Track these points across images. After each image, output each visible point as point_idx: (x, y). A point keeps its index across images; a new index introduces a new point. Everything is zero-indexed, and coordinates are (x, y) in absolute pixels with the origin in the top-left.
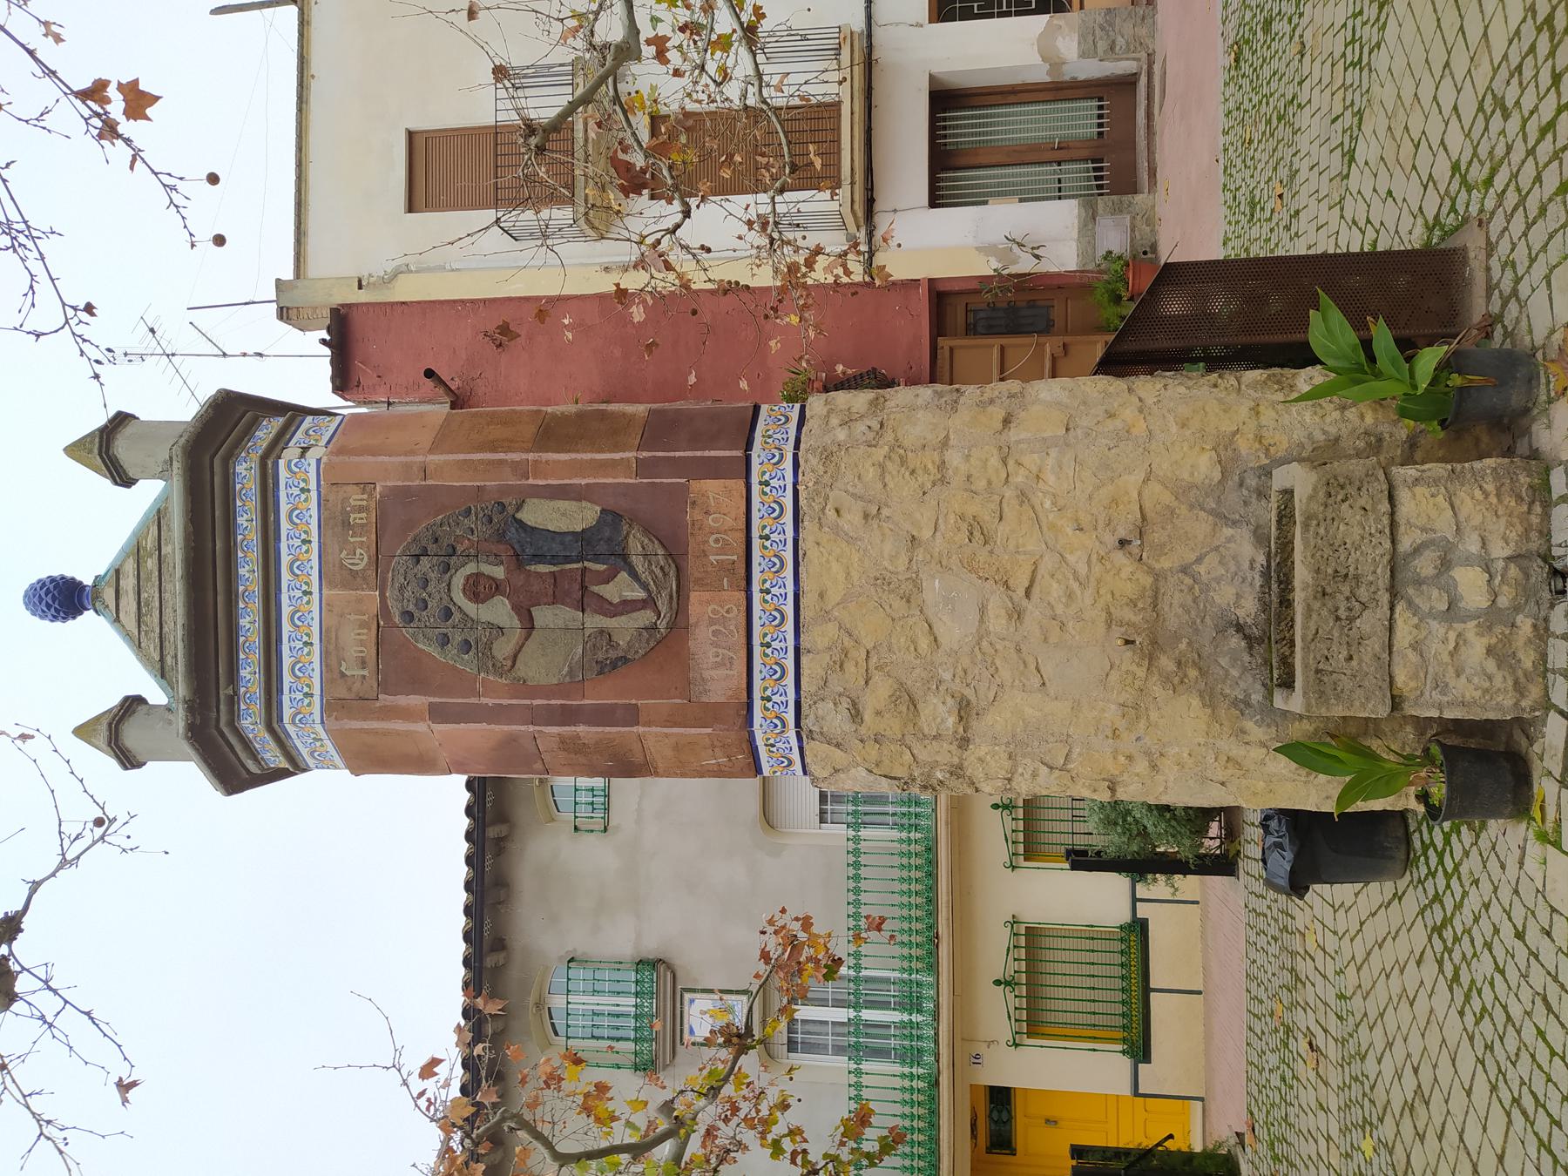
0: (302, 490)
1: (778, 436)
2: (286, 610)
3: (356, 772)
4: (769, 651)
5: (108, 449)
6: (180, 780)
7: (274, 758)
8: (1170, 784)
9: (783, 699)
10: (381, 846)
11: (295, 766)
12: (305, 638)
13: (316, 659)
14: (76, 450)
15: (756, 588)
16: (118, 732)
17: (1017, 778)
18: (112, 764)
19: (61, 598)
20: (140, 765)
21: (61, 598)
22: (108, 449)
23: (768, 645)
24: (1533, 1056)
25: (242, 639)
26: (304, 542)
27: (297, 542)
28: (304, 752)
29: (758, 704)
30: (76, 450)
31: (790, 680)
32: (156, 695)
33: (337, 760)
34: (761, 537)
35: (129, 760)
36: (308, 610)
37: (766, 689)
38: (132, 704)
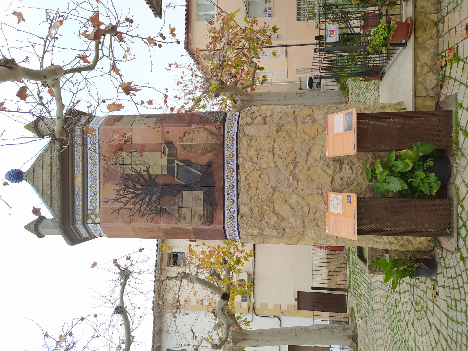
1: (233, 119)
2: (89, 170)
3: (111, 236)
4: (229, 196)
6: (58, 240)
11: (92, 237)
12: (94, 178)
14: (27, 227)
15: (226, 209)
18: (35, 237)
19: (16, 176)
20: (43, 236)
21: (16, 176)
25: (76, 193)
26: (95, 179)
27: (93, 180)
29: (226, 165)
31: (235, 189)
34: (227, 147)
35: (40, 235)
36: (95, 190)
37: (228, 191)
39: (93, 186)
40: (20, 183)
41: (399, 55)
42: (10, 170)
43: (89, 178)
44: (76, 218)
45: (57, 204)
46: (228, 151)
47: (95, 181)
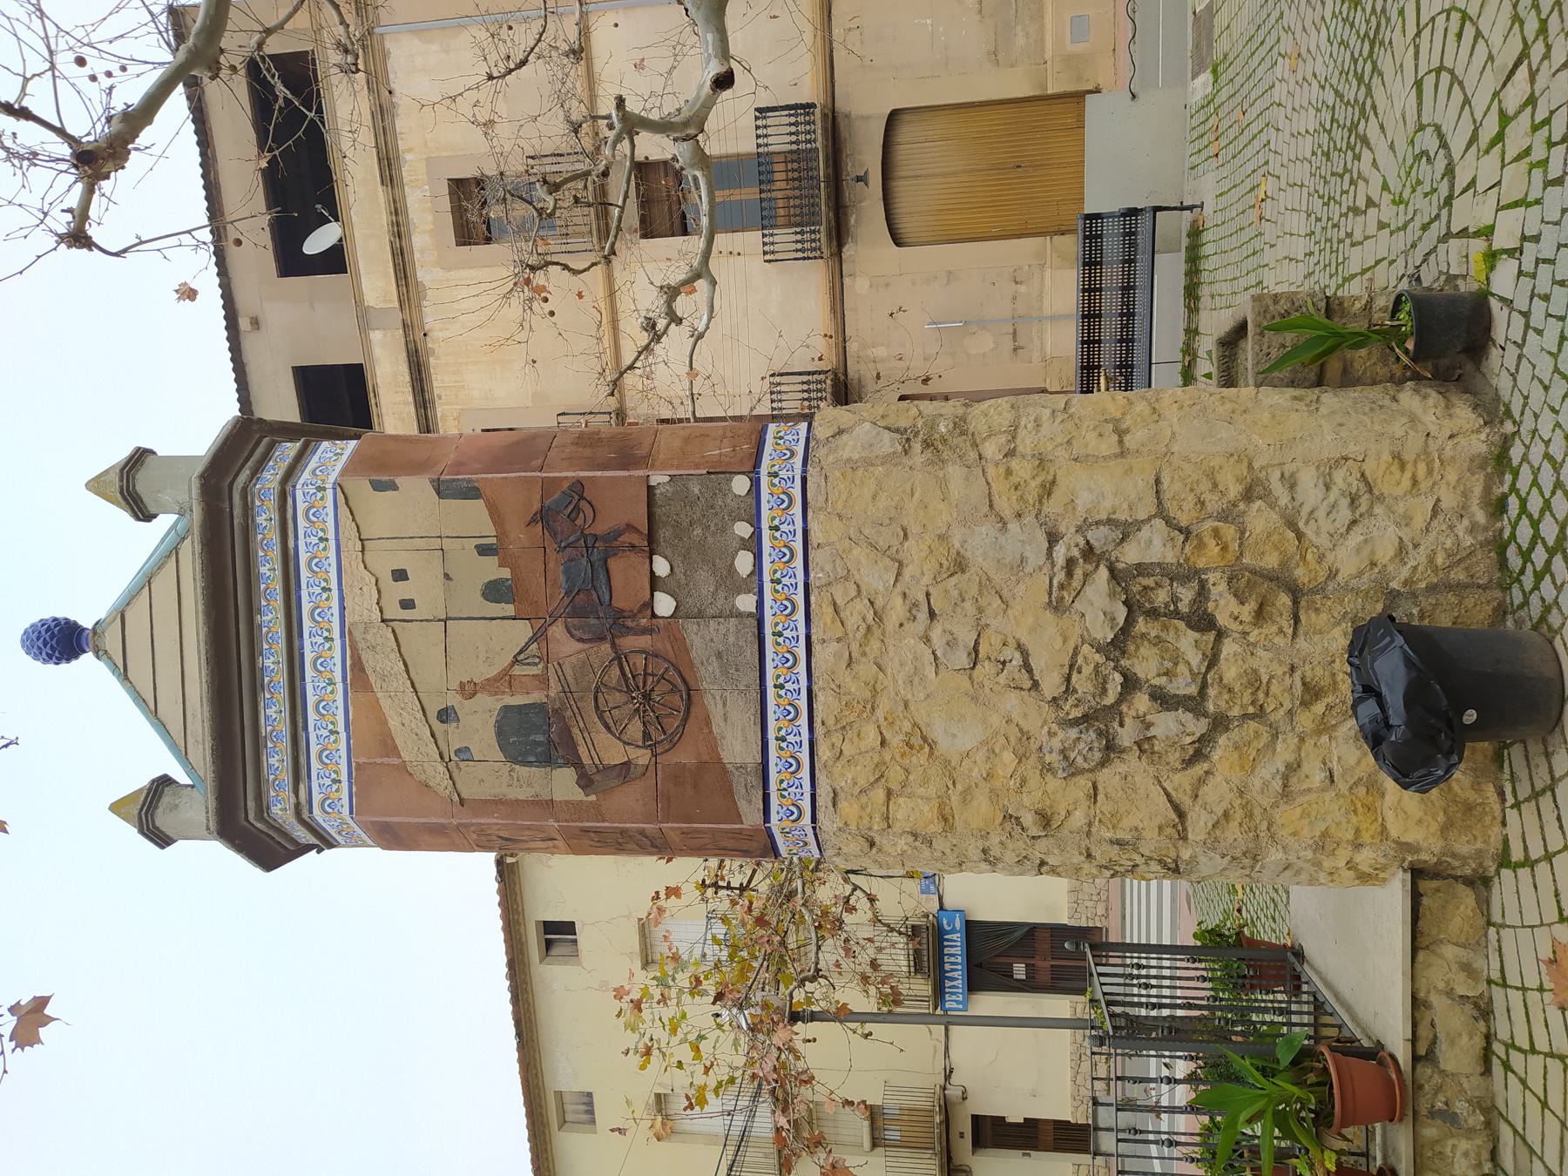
0: (321, 539)
1: (789, 437)
5: (130, 482)
6: (212, 859)
7: (309, 838)
8: (1176, 428)
9: (793, 581)
10: (409, 925)
13: (345, 795)
14: (97, 485)
16: (150, 812)
17: (1022, 433)
18: (122, 517)
19: (60, 641)
21: (60, 641)
22: (130, 482)
23: (778, 582)
24: (1523, 1082)
26: (334, 781)
27: (317, 590)
28: (332, 832)
30: (97, 485)
32: (181, 777)
33: (369, 842)
35: (162, 840)
37: (777, 624)
38: (164, 782)
39: (326, 755)
40: (74, 662)
41: (1337, 995)
42: (35, 619)
43: (304, 586)
44: (260, 520)
45: (201, 750)
46: (774, 485)
47: (325, 595)
